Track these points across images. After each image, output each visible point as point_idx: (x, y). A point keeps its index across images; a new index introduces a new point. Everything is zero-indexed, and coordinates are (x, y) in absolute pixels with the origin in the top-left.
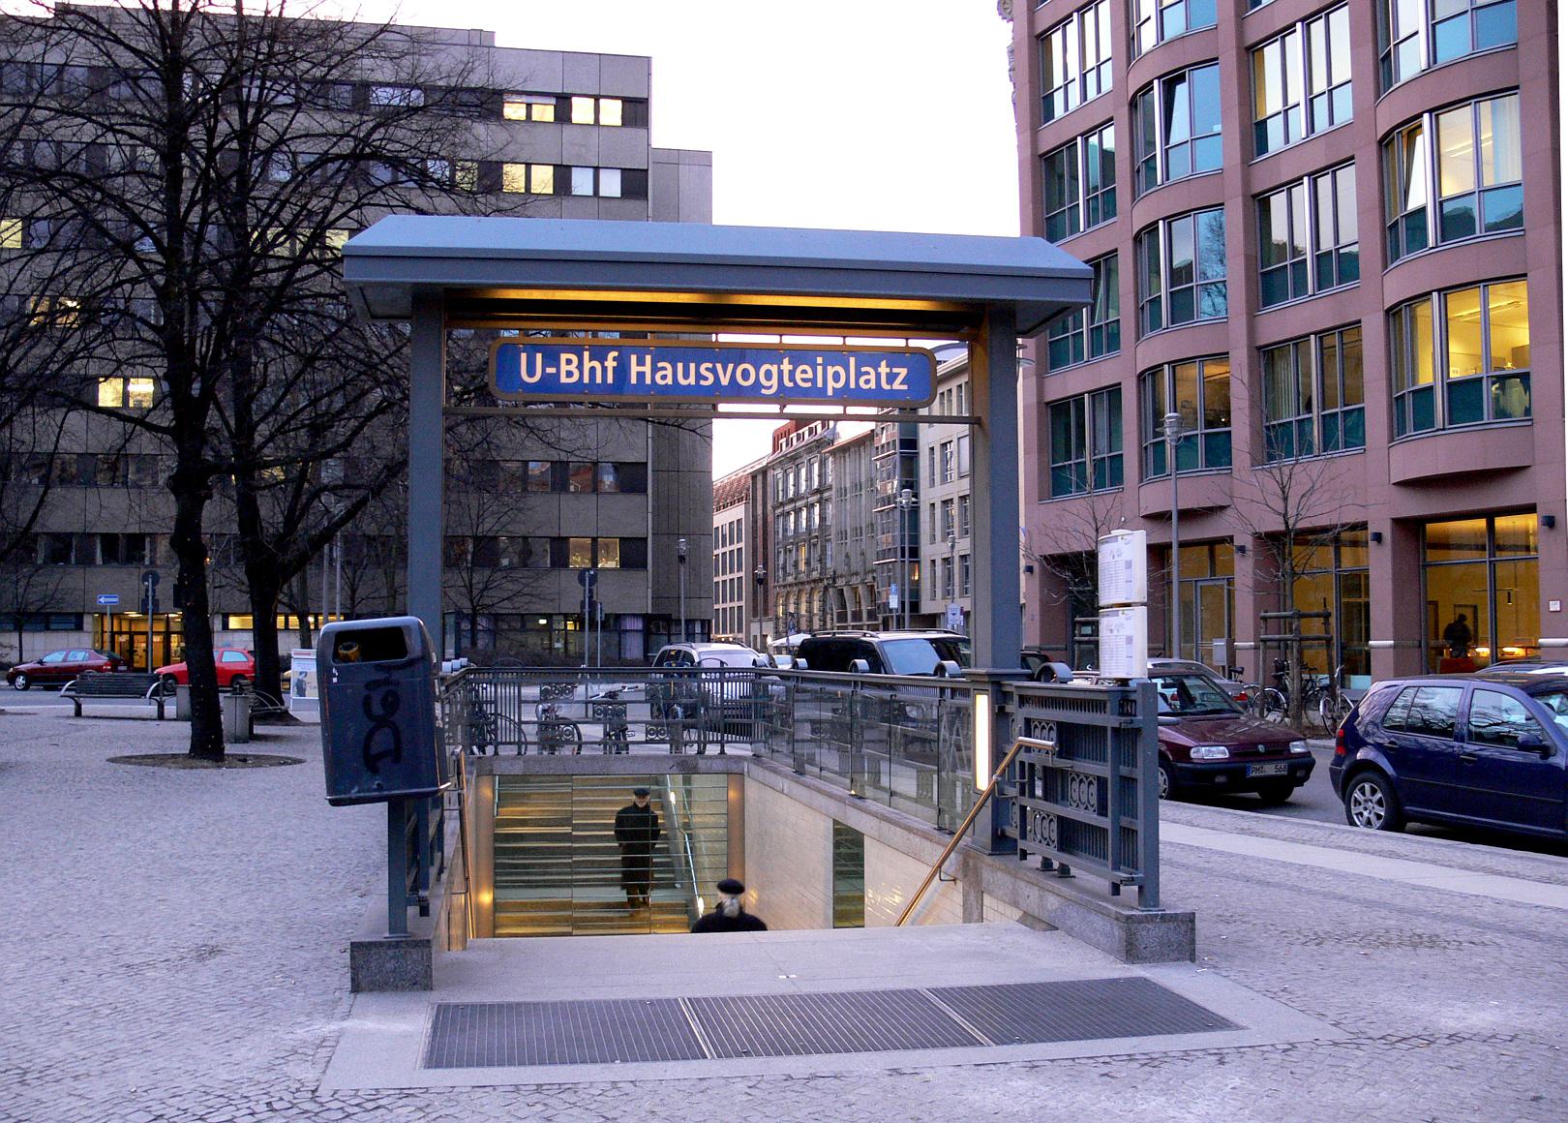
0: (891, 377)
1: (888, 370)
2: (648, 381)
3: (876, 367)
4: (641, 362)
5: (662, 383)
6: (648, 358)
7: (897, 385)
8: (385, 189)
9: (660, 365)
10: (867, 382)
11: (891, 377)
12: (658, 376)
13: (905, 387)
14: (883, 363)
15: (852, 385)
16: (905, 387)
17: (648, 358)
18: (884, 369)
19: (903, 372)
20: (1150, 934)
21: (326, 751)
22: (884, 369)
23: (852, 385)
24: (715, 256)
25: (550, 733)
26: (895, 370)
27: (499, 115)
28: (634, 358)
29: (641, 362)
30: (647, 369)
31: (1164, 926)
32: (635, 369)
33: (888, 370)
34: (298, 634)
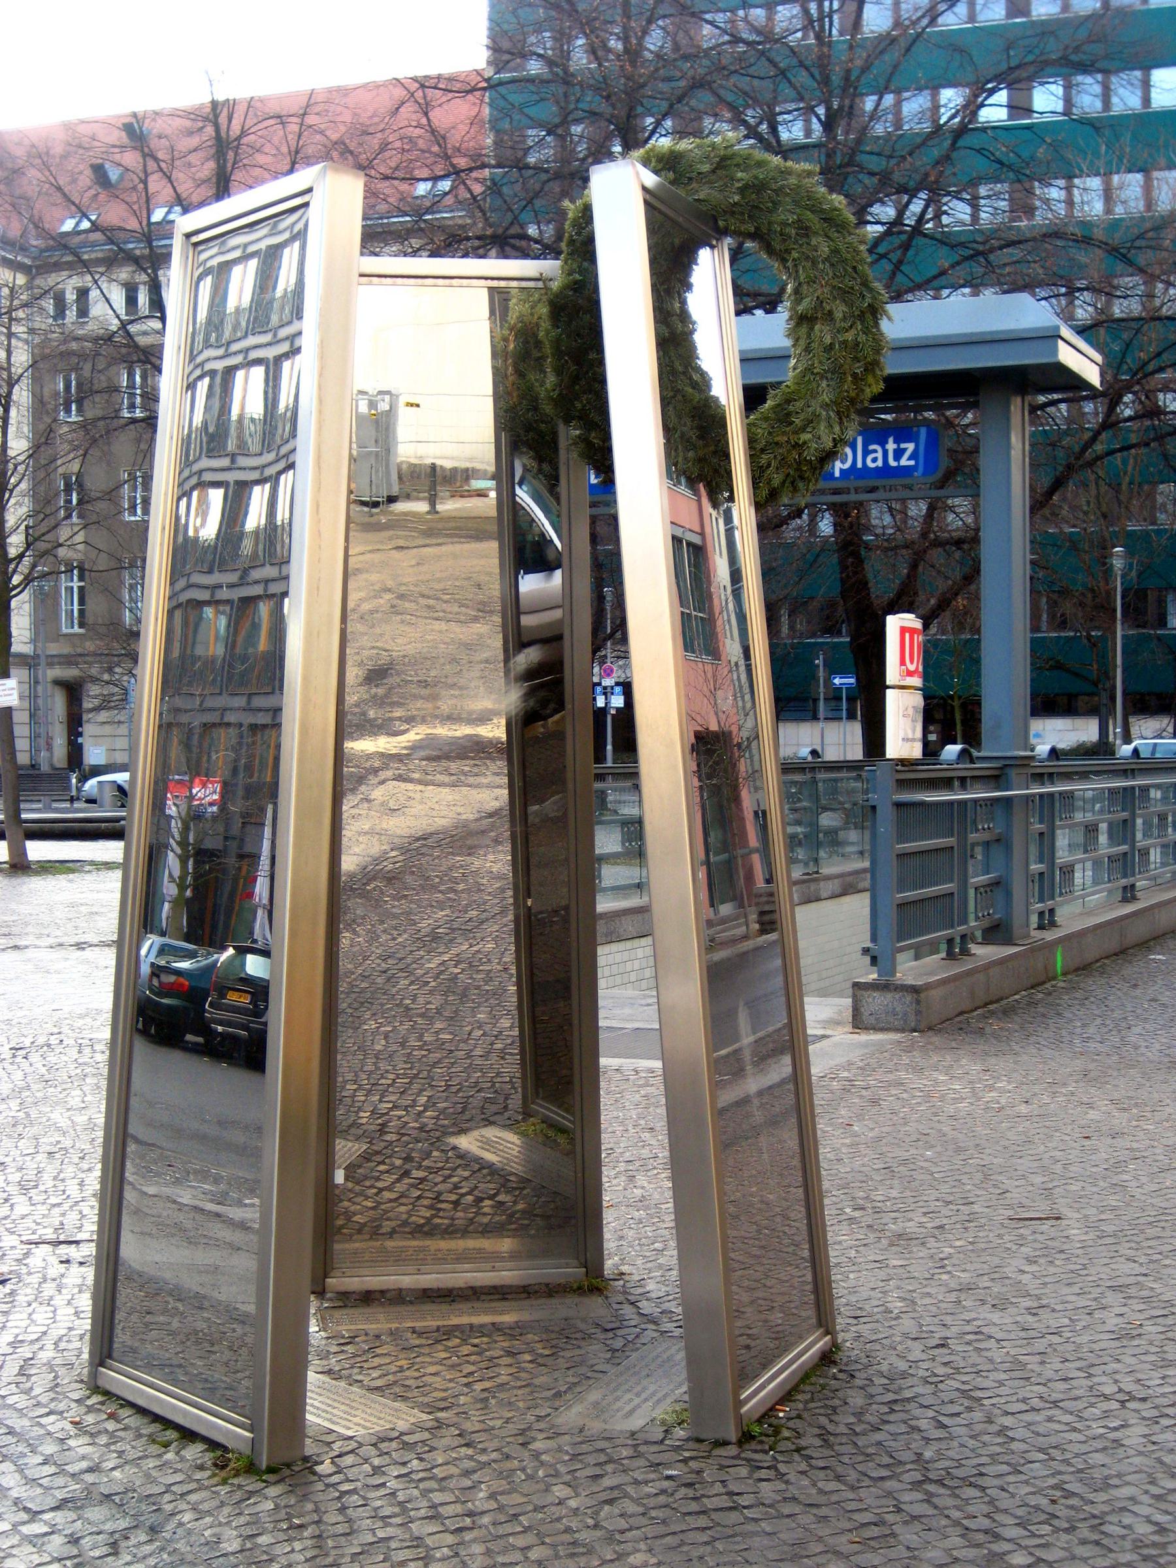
0: (898, 454)
3: (883, 444)
5: (872, 465)
7: (904, 462)
8: (546, 189)
9: (871, 447)
10: (874, 460)
11: (898, 454)
12: (869, 459)
13: (912, 463)
14: (891, 440)
15: (859, 465)
16: (912, 463)
18: (891, 446)
19: (910, 447)
20: (876, 1002)
21: (599, 1132)
22: (891, 446)
23: (859, 465)
24: (761, 350)
25: (767, 918)
26: (903, 446)
27: (183, 1041)
31: (889, 996)
34: (501, 765)
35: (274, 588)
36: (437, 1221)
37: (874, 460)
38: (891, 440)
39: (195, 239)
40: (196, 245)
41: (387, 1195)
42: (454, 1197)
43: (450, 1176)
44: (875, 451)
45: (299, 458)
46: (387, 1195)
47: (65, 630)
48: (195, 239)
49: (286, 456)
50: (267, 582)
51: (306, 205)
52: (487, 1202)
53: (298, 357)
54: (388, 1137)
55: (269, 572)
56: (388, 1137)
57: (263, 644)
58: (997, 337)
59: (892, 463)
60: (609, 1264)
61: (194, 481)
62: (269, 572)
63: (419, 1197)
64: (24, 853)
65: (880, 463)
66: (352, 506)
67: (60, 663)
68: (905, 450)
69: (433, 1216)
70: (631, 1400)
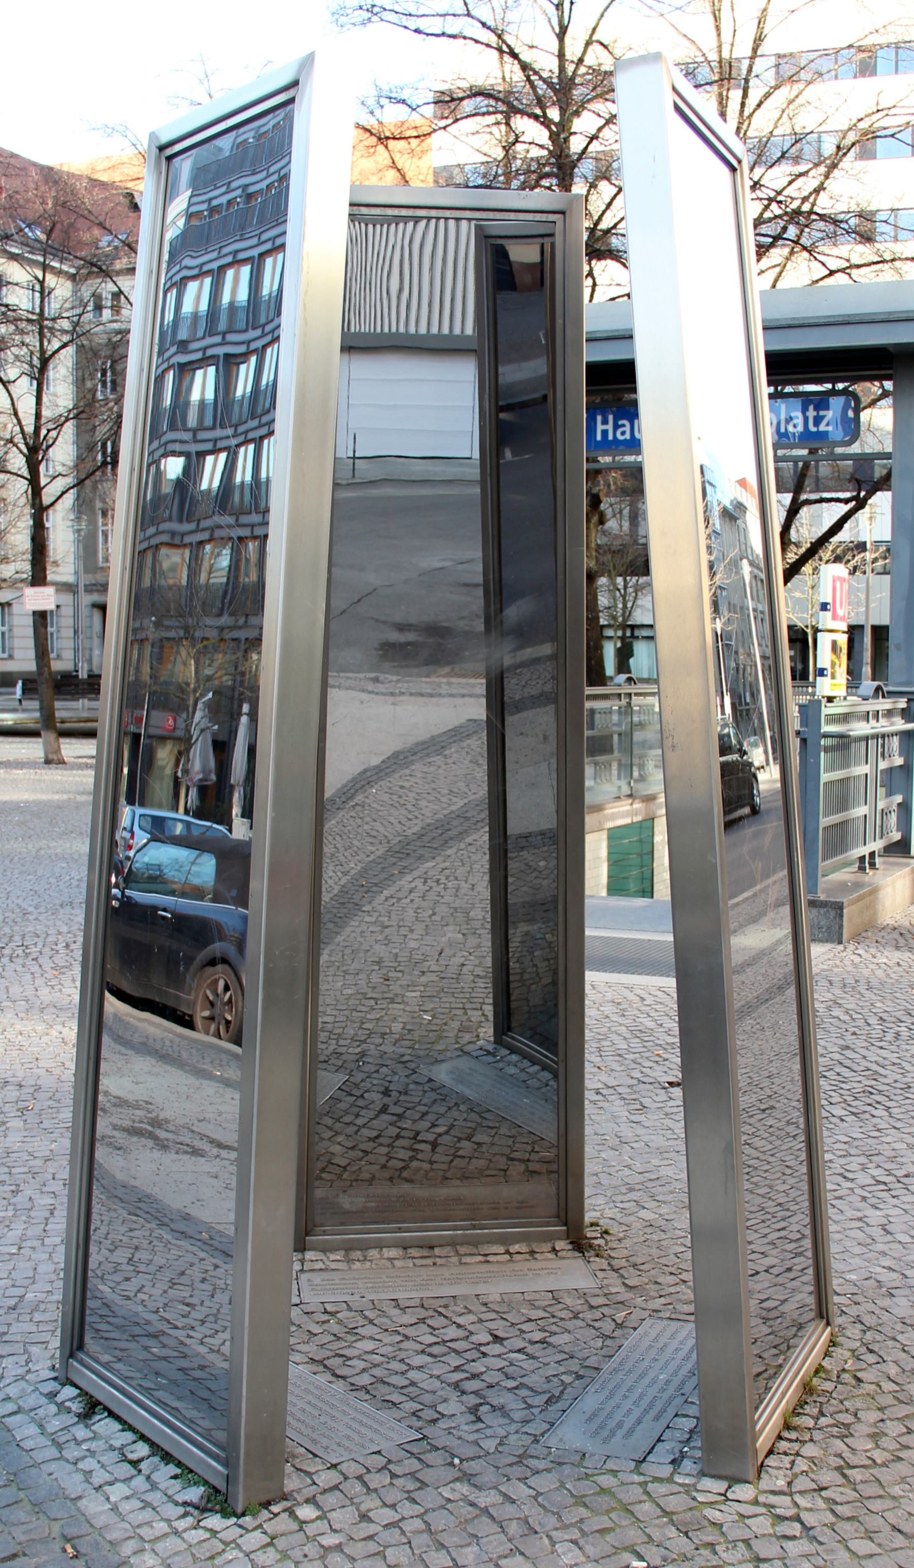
1: (815, 413)
2: (610, 437)
4: (605, 422)
6: (611, 418)
9: (620, 422)
14: (811, 408)
17: (611, 418)
26: (822, 413)
28: (599, 418)
29: (605, 422)
30: (610, 427)
32: (600, 427)
33: (815, 413)
35: (258, 531)
37: (623, 433)
38: (811, 408)
41: (365, 1132)
42: (431, 1137)
43: (427, 1113)
44: (623, 426)
45: (278, 426)
46: (365, 1132)
47: (101, 565)
49: (273, 331)
50: (252, 526)
51: (292, 101)
54: (367, 1068)
55: (255, 518)
56: (367, 1068)
57: (254, 577)
58: (892, 317)
59: (812, 429)
60: (589, 1217)
61: (161, 451)
62: (255, 518)
63: (398, 1137)
64: (58, 750)
66: (649, 621)
67: (98, 591)
68: (824, 417)
69: (412, 1158)
70: (629, 1411)
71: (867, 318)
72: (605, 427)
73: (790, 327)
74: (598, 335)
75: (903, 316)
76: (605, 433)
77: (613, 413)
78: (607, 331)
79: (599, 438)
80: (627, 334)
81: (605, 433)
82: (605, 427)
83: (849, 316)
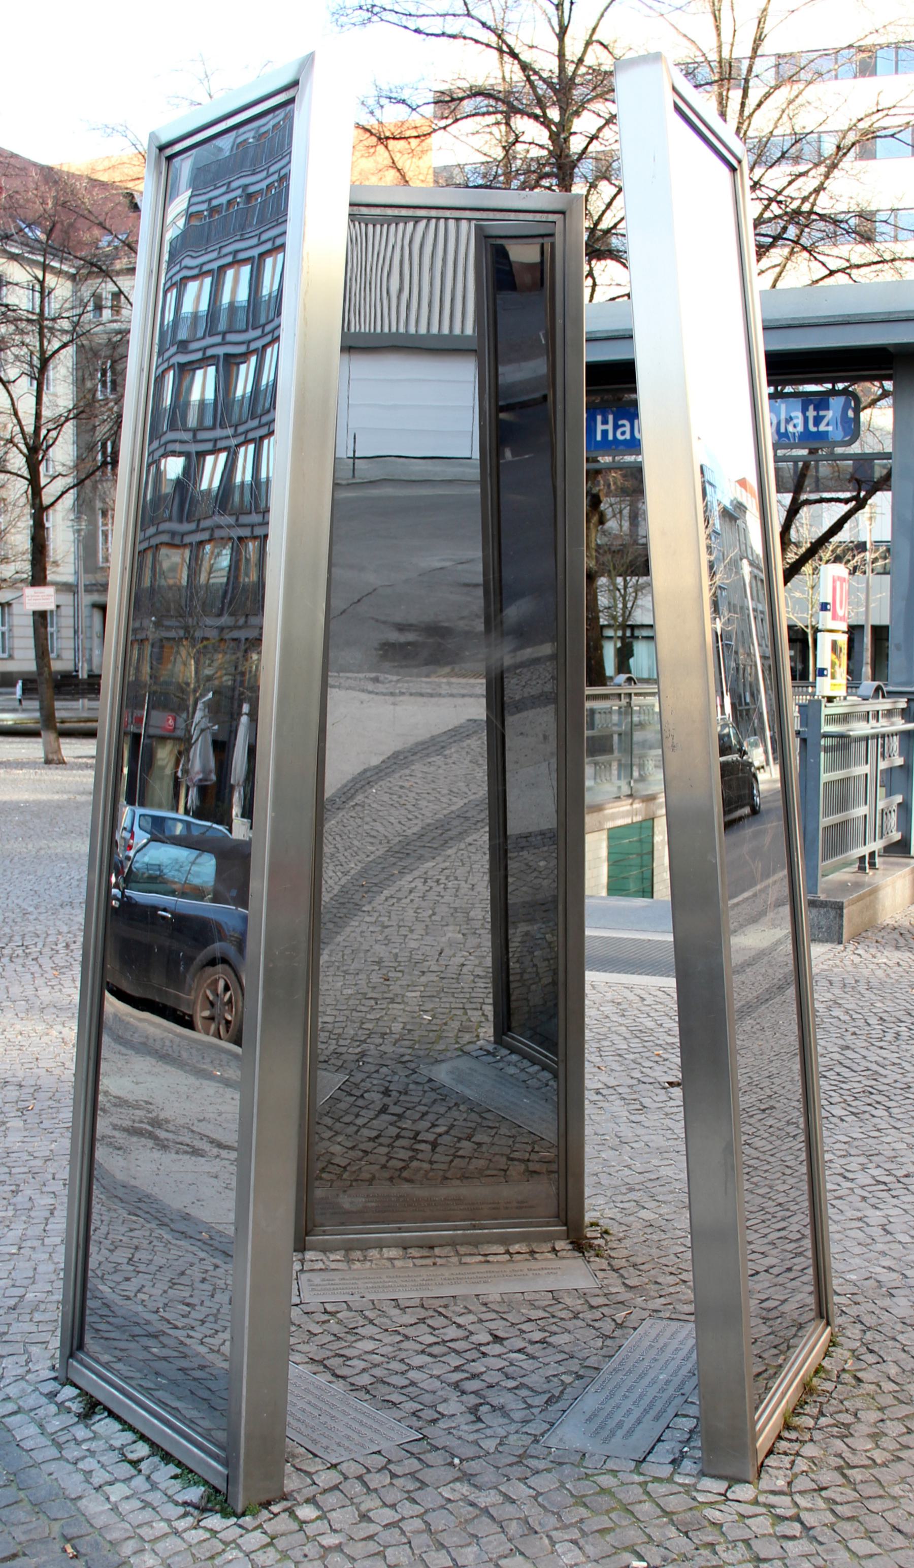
1: (815, 413)
2: (610, 437)
4: (605, 422)
6: (611, 418)
9: (620, 422)
14: (811, 408)
17: (611, 418)
26: (822, 413)
28: (599, 418)
29: (605, 422)
30: (610, 427)
32: (600, 427)
33: (815, 413)
35: (258, 531)
36: (415, 1164)
37: (623, 433)
38: (811, 408)
39: (169, 152)
40: (169, 159)
41: (365, 1132)
42: (431, 1137)
43: (427, 1113)
44: (623, 426)
45: (278, 426)
46: (365, 1132)
48: (169, 152)
49: (273, 331)
50: (252, 526)
51: (292, 101)
52: (465, 1144)
53: (272, 439)
55: (255, 518)
56: (367, 1068)
57: (254, 577)
58: (892, 317)
59: (812, 429)
60: (589, 1217)
62: (255, 518)
65: (628, 436)
68: (824, 417)
70: (629, 1411)
71: (867, 318)
72: (605, 427)
73: (790, 327)
74: (598, 335)
75: (903, 316)
76: (605, 433)
77: (613, 413)
78: (607, 331)
79: (599, 438)
80: (627, 334)
81: (605, 433)
82: (605, 427)
83: (849, 316)
